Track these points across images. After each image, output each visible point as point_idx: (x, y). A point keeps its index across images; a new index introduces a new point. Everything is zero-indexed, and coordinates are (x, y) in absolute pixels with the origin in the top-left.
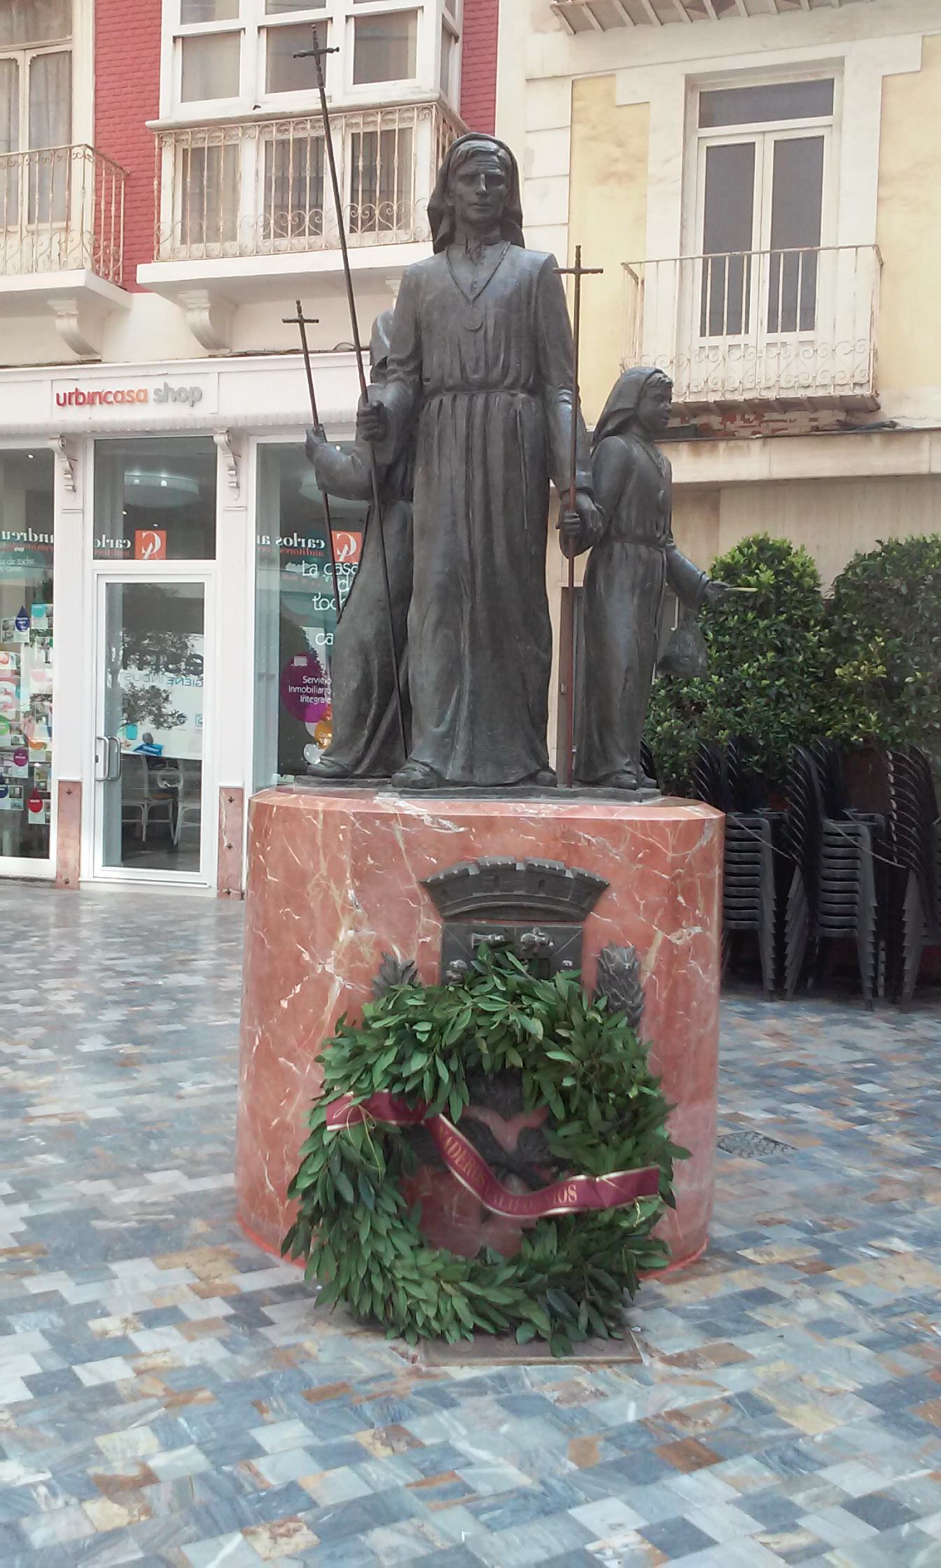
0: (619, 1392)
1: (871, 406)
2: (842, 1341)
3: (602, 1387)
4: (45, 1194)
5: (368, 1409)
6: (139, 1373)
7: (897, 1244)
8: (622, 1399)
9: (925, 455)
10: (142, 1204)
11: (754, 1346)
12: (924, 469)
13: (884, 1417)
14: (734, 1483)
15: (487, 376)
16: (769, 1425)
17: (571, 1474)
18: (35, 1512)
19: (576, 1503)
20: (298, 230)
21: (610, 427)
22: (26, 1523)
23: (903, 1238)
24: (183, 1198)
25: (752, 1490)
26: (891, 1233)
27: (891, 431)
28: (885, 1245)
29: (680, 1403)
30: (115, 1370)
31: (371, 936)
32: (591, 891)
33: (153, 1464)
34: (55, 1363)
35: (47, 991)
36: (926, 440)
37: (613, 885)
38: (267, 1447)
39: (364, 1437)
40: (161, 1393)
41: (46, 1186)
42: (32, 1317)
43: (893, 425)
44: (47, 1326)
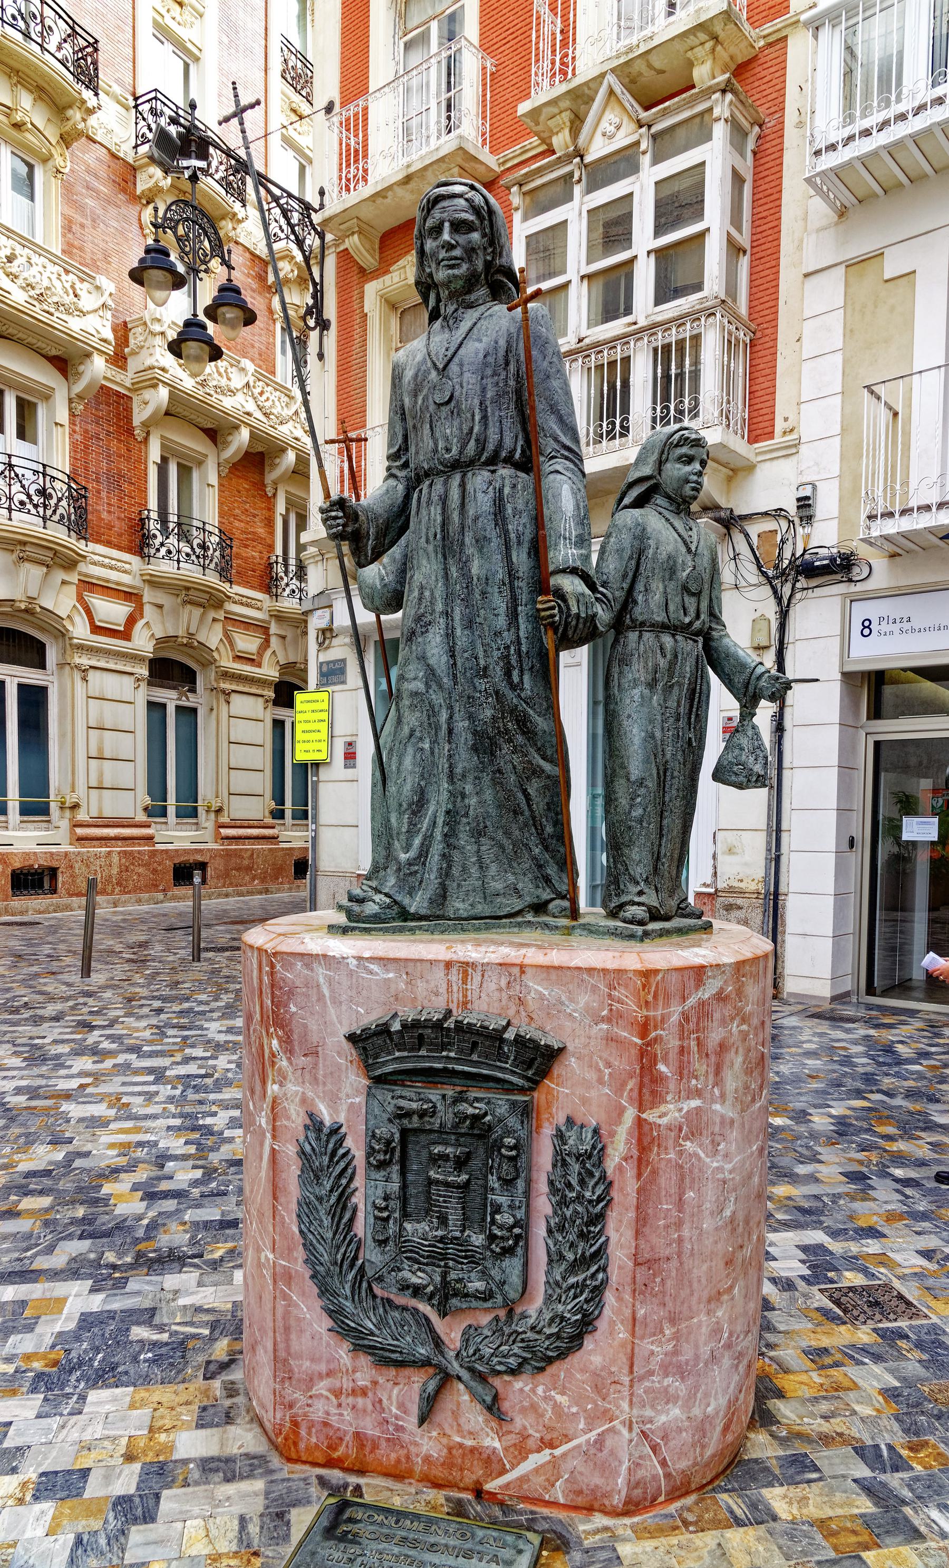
15: (461, 453)
20: (611, 435)
21: (626, 501)
31: (297, 1092)
32: (539, 1060)
37: (570, 1047)
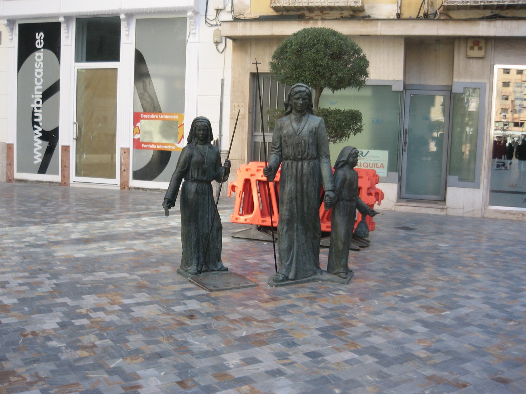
0: (241, 329)
1: (361, 10)
2: (316, 316)
3: (236, 328)
4: (61, 277)
5: (162, 332)
6: (91, 322)
7: (341, 292)
8: (242, 330)
9: (379, 28)
10: (92, 280)
11: (286, 318)
12: (379, 33)
13: (322, 335)
14: (271, 349)
16: (287, 336)
17: (223, 347)
18: (62, 352)
19: (223, 353)
22: (60, 355)
23: (343, 291)
24: (106, 279)
25: (277, 351)
26: (340, 290)
27: (368, 19)
28: (337, 293)
29: (260, 331)
30: (84, 322)
33: (96, 343)
34: (66, 320)
35: (58, 219)
36: (379, 23)
38: (131, 340)
39: (161, 338)
40: (98, 327)
41: (61, 275)
42: (59, 309)
43: (369, 17)
44: (63, 310)
